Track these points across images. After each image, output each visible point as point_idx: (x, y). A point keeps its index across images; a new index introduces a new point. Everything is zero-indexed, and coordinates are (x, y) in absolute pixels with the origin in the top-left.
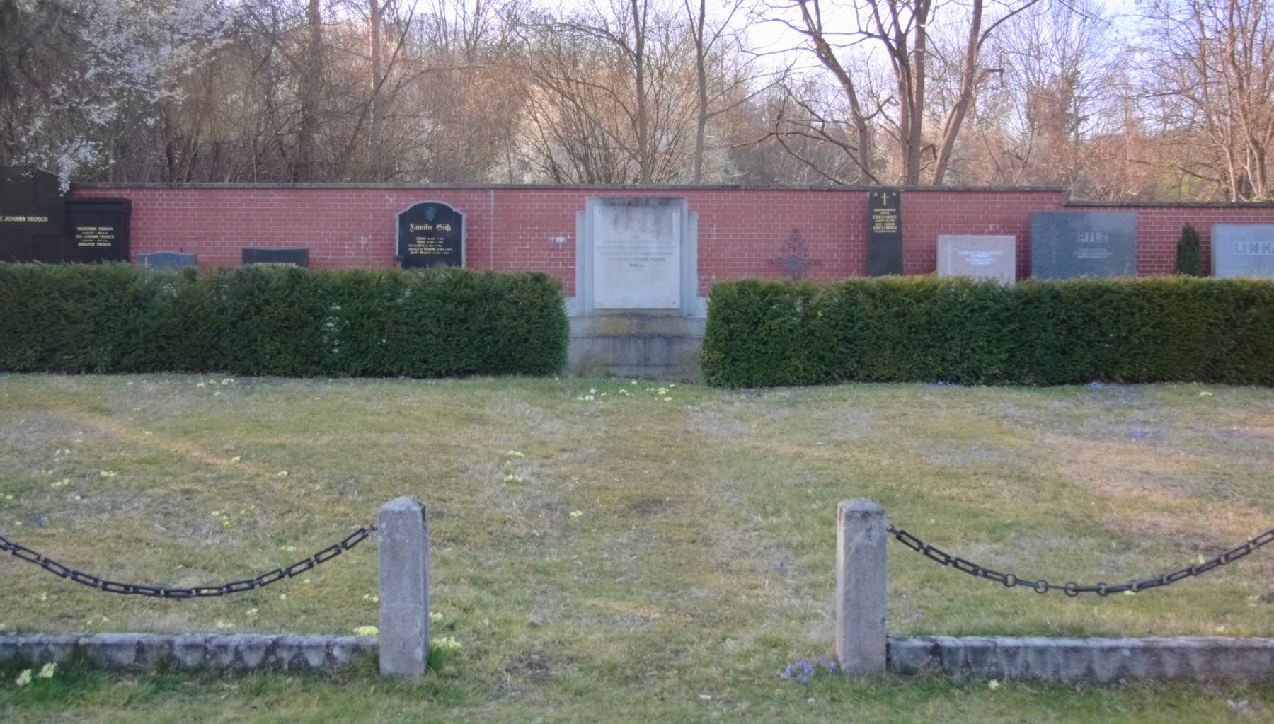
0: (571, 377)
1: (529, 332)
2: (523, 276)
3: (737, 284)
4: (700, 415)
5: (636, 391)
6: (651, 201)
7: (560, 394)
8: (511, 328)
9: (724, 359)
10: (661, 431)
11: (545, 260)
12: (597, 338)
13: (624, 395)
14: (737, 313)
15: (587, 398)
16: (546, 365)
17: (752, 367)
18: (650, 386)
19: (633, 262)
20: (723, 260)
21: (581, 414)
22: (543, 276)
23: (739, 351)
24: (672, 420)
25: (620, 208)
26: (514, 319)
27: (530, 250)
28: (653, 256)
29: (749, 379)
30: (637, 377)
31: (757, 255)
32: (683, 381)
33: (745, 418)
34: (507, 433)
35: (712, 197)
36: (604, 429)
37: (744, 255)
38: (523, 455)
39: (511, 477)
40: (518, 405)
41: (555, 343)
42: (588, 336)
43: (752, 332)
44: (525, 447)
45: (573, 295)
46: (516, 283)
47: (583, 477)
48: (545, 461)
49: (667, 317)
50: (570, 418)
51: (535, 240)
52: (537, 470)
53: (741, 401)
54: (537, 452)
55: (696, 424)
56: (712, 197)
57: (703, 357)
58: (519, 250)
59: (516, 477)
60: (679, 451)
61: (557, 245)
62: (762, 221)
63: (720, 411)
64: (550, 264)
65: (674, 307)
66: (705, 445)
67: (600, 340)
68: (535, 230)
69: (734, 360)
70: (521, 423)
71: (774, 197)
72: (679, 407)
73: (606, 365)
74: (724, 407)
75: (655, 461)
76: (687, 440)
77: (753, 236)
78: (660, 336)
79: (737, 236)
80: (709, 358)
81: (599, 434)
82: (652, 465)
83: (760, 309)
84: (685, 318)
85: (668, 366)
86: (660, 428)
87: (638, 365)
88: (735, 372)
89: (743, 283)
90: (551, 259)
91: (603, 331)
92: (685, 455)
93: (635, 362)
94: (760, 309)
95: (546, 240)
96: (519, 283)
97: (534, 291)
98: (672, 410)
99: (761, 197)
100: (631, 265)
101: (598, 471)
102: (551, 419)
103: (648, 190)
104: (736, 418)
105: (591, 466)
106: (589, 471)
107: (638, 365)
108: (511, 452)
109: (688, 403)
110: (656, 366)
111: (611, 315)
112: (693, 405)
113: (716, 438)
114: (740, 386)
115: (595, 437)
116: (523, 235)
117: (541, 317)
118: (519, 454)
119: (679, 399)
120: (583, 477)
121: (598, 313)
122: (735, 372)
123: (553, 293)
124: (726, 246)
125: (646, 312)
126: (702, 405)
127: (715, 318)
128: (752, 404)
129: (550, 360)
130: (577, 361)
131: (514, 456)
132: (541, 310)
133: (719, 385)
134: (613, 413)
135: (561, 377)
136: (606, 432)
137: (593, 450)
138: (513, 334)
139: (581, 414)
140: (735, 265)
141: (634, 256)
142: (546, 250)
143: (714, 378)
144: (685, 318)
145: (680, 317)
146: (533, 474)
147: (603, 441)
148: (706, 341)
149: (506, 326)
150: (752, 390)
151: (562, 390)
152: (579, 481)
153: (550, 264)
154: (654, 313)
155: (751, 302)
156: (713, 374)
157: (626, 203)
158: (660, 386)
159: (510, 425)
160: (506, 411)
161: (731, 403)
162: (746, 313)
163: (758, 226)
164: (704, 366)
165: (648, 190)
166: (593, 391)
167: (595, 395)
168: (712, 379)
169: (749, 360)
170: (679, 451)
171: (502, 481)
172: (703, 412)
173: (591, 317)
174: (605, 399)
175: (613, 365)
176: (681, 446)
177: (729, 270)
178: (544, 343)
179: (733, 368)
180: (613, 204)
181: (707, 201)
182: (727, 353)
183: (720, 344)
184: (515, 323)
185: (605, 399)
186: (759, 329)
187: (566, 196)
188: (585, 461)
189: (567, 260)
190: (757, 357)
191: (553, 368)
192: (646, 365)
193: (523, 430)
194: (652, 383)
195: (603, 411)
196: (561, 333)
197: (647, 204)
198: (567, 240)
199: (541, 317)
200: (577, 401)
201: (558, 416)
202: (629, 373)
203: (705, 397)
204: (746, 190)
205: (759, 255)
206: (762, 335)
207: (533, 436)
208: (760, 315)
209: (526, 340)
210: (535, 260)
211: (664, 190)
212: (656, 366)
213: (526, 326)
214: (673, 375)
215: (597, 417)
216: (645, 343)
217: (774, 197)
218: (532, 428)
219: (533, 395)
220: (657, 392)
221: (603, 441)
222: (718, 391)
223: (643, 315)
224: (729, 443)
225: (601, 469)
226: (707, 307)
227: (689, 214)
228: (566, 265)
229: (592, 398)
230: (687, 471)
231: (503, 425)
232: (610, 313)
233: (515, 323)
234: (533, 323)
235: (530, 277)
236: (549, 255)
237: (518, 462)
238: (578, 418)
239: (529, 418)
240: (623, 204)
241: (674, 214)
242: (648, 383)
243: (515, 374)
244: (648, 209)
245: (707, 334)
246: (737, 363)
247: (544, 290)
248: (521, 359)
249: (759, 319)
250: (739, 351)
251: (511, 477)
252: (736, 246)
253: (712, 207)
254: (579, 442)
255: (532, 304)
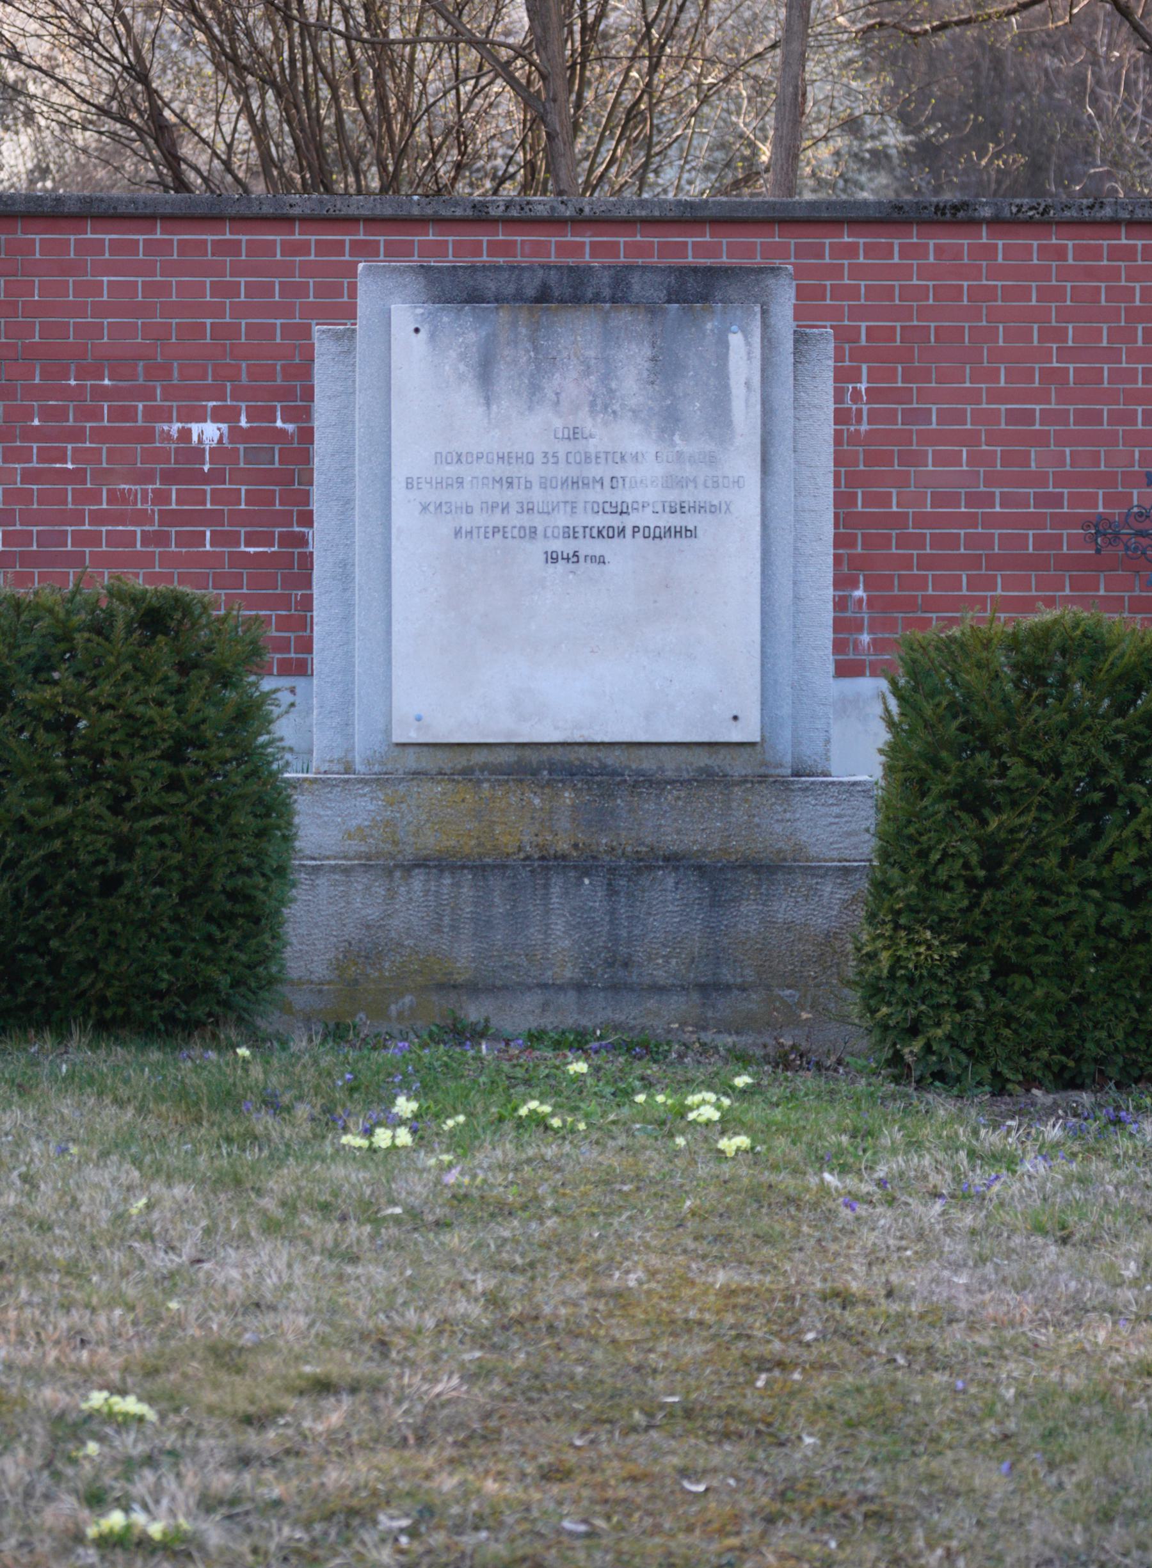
0: (299, 1043)
1: (124, 847)
2: (93, 607)
3: (1014, 643)
4: (885, 1217)
5: (592, 1106)
6: (635, 280)
7: (264, 1122)
8: (47, 834)
9: (963, 962)
10: (729, 1293)
11: (142, 518)
12: (408, 869)
13: (540, 1122)
14: (1017, 767)
15: (383, 1137)
16: (193, 991)
17: (1080, 1000)
18: (648, 1084)
19: (559, 545)
20: (899, 520)
21: (369, 1212)
22: (179, 603)
23: (1023, 930)
24: (767, 1239)
25: (503, 315)
26: (60, 796)
27: (77, 476)
28: (644, 519)
29: (1066, 1050)
30: (579, 1043)
31: (1043, 500)
32: (783, 1061)
33: (1082, 1230)
34: (66, 1307)
35: (852, 250)
36: (481, 1283)
37: (988, 499)
38: (151, 1415)
39: (116, 1519)
40: (91, 1173)
41: (233, 895)
42: (368, 863)
43: (1080, 849)
44: (152, 1372)
45: (302, 669)
46: (64, 636)
47: (427, 1512)
48: (252, 1440)
49: (708, 778)
50: (328, 1232)
51: (100, 435)
52: (223, 1481)
53: (1047, 1152)
54: (210, 1397)
55: (874, 1260)
56: (852, 250)
57: (872, 957)
58: (29, 476)
59: (139, 1518)
60: (821, 1387)
61: (197, 453)
62: (1065, 354)
63: (963, 1197)
64: (160, 539)
65: (736, 735)
66: (933, 1361)
67: (418, 882)
68: (101, 393)
69: (1003, 967)
70: (117, 1258)
71: (1116, 253)
72: (786, 1181)
73: (447, 986)
74: (977, 1178)
75: (726, 1435)
76: (847, 1335)
77: (1027, 417)
78: (673, 860)
79: (960, 417)
80: (897, 961)
81: (462, 1306)
82: (716, 1458)
83: (1113, 748)
84: (783, 786)
85: (709, 989)
86: (721, 1277)
87: (580, 988)
88: (1009, 1019)
89: (1042, 636)
90: (168, 518)
91: (431, 842)
92: (852, 1407)
93: (569, 973)
94: (1113, 748)
95: (147, 435)
96: (79, 638)
97: (146, 673)
98: (758, 1195)
99: (1060, 252)
100: (553, 558)
101: (491, 1486)
102: (244, 1237)
103: (580, 221)
104: (1039, 1229)
105: (454, 1463)
106: (448, 1483)
107: (580, 988)
108: (97, 1399)
109: (822, 1162)
110: (658, 989)
111: (467, 772)
112: (844, 1170)
113: (971, 1328)
114: (1030, 1082)
115: (444, 1325)
116: (47, 414)
117: (174, 784)
118: (131, 1405)
119: (782, 1143)
120: (427, 1512)
121: (411, 760)
122: (1009, 1019)
123: (225, 679)
124: (912, 459)
125: (612, 759)
126: (881, 1172)
127: (921, 787)
128: (1096, 1166)
129: (213, 972)
130: (320, 971)
131: (110, 1417)
132: (175, 756)
133: (940, 1076)
134: (503, 1211)
135: (255, 1040)
136: (493, 1300)
137: (448, 1385)
138: (52, 858)
139: (369, 1212)
140: (953, 541)
141: (562, 520)
142: (146, 477)
143: (917, 1046)
144: (783, 786)
145: (763, 778)
146: (207, 1504)
147: (481, 1338)
148: (882, 887)
149: (21, 825)
150: (1086, 1098)
151: (271, 1103)
152: (412, 1532)
153: (160, 539)
154: (647, 762)
155: (1074, 721)
156: (914, 1030)
157: (530, 292)
158: (690, 1084)
159: (73, 1269)
160: (44, 1203)
161: (1009, 1161)
162: (1055, 767)
163: (1049, 375)
164: (875, 991)
165: (580, 221)
166: (405, 1106)
167: (415, 1124)
168: (912, 1050)
169: (1066, 972)
170: (821, 1387)
171: (79, 1538)
172: (891, 1201)
173: (381, 781)
174: (463, 1143)
175: (474, 989)
176: (820, 1366)
177: (926, 563)
178: (185, 896)
179: (1000, 1004)
180: (474, 297)
181: (835, 271)
182: (973, 941)
183: (945, 902)
184: (63, 813)
185: (463, 1143)
186: (1112, 836)
187: (232, 248)
188: (422, 1439)
189: (239, 518)
190: (1102, 955)
191: (226, 1004)
192: (615, 988)
193: (131, 1291)
194: (653, 1070)
195: (460, 1198)
196: (259, 856)
197: (619, 296)
198: (236, 433)
199: (174, 784)
200: (343, 1154)
201: (271, 1227)
202: (549, 1021)
203: (892, 1135)
204: (996, 222)
205: (1056, 500)
206: (1120, 862)
207: (179, 1323)
208: (1116, 774)
209: (111, 884)
210: (98, 518)
211: (646, 221)
212: (658, 989)
213: (111, 822)
214: (725, 1027)
215: (441, 1225)
216: (612, 891)
217: (1116, 253)
218: (169, 1281)
219: (150, 1125)
220: (682, 1111)
221: (481, 1338)
222: (943, 1106)
223: (604, 770)
224: (1032, 1350)
225: (501, 1476)
226: (884, 736)
227: (800, 339)
228: (231, 539)
229: (404, 1137)
230: (874, 1480)
231: (43, 1266)
232: (461, 760)
233: (63, 813)
234: (142, 812)
235: (123, 613)
236: (161, 497)
237: (131, 1444)
238: (360, 1232)
239: (148, 1236)
240: (519, 297)
241: (736, 340)
242: (639, 1068)
243: (62, 1035)
244: (624, 316)
245: (885, 855)
246: (1019, 981)
247: (183, 668)
248: (92, 964)
249: (1111, 794)
250: (1023, 930)
251: (116, 1519)
252: (955, 459)
253: (854, 292)
254: (383, 1346)
255: (134, 727)
